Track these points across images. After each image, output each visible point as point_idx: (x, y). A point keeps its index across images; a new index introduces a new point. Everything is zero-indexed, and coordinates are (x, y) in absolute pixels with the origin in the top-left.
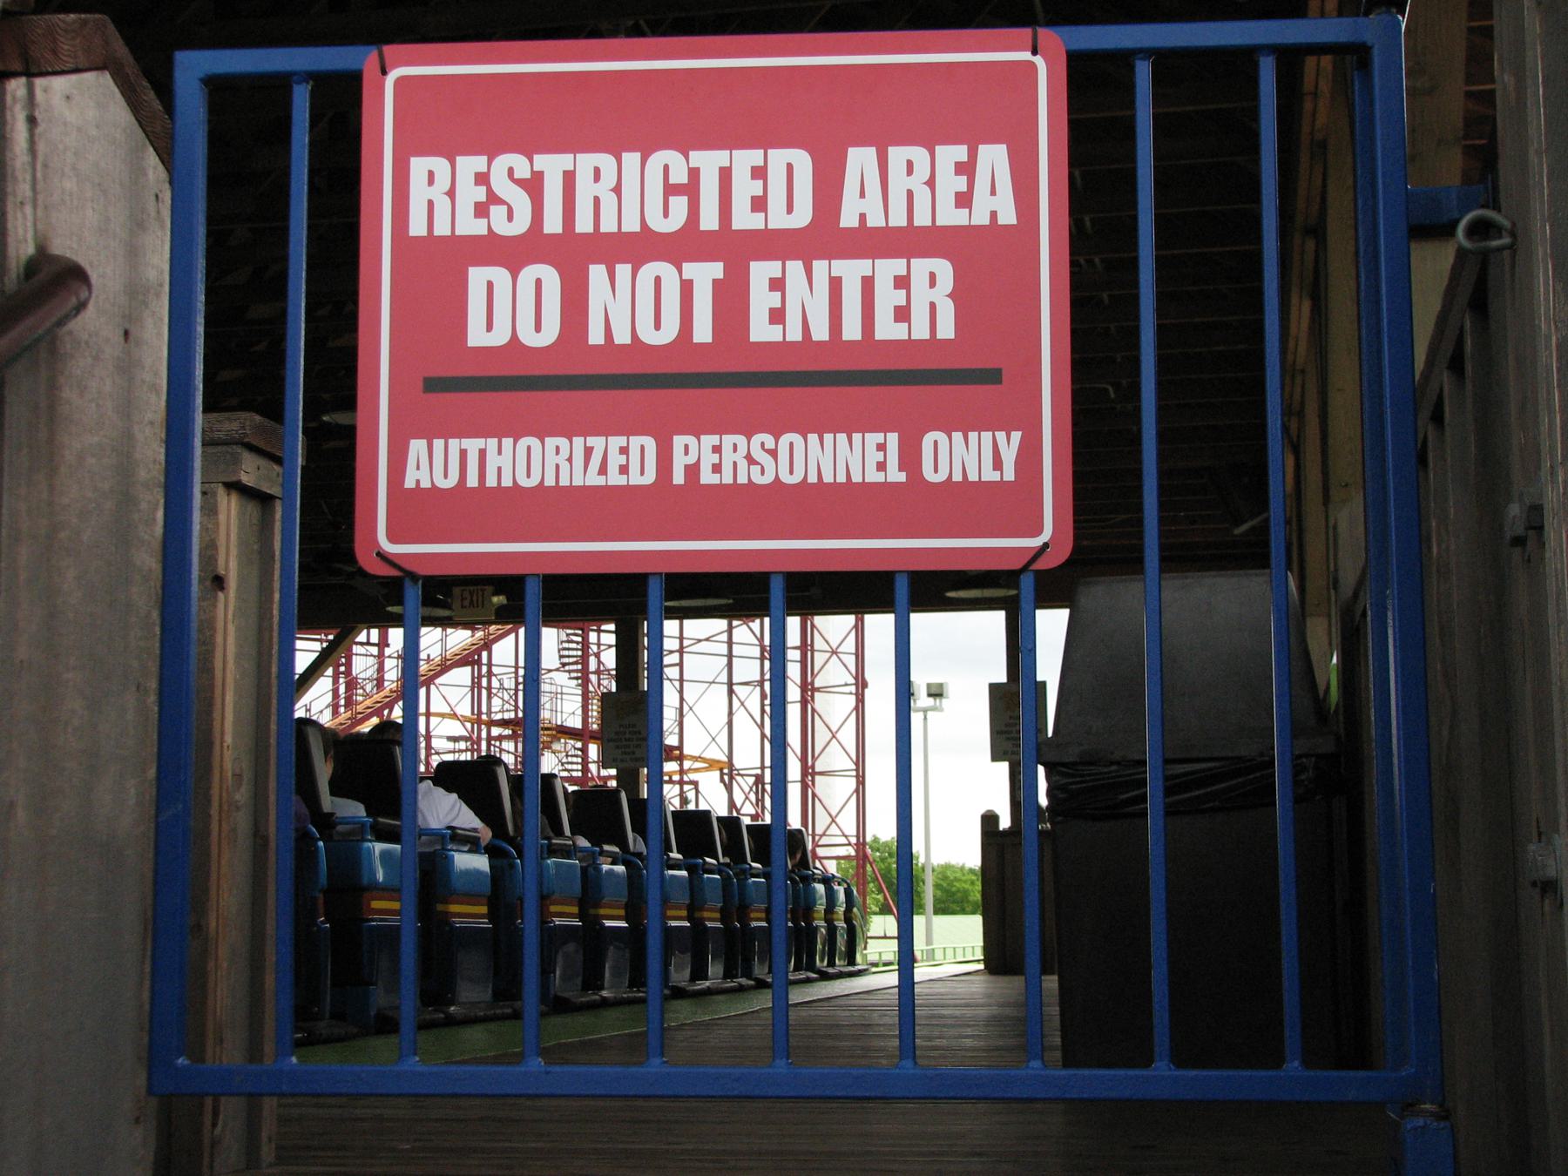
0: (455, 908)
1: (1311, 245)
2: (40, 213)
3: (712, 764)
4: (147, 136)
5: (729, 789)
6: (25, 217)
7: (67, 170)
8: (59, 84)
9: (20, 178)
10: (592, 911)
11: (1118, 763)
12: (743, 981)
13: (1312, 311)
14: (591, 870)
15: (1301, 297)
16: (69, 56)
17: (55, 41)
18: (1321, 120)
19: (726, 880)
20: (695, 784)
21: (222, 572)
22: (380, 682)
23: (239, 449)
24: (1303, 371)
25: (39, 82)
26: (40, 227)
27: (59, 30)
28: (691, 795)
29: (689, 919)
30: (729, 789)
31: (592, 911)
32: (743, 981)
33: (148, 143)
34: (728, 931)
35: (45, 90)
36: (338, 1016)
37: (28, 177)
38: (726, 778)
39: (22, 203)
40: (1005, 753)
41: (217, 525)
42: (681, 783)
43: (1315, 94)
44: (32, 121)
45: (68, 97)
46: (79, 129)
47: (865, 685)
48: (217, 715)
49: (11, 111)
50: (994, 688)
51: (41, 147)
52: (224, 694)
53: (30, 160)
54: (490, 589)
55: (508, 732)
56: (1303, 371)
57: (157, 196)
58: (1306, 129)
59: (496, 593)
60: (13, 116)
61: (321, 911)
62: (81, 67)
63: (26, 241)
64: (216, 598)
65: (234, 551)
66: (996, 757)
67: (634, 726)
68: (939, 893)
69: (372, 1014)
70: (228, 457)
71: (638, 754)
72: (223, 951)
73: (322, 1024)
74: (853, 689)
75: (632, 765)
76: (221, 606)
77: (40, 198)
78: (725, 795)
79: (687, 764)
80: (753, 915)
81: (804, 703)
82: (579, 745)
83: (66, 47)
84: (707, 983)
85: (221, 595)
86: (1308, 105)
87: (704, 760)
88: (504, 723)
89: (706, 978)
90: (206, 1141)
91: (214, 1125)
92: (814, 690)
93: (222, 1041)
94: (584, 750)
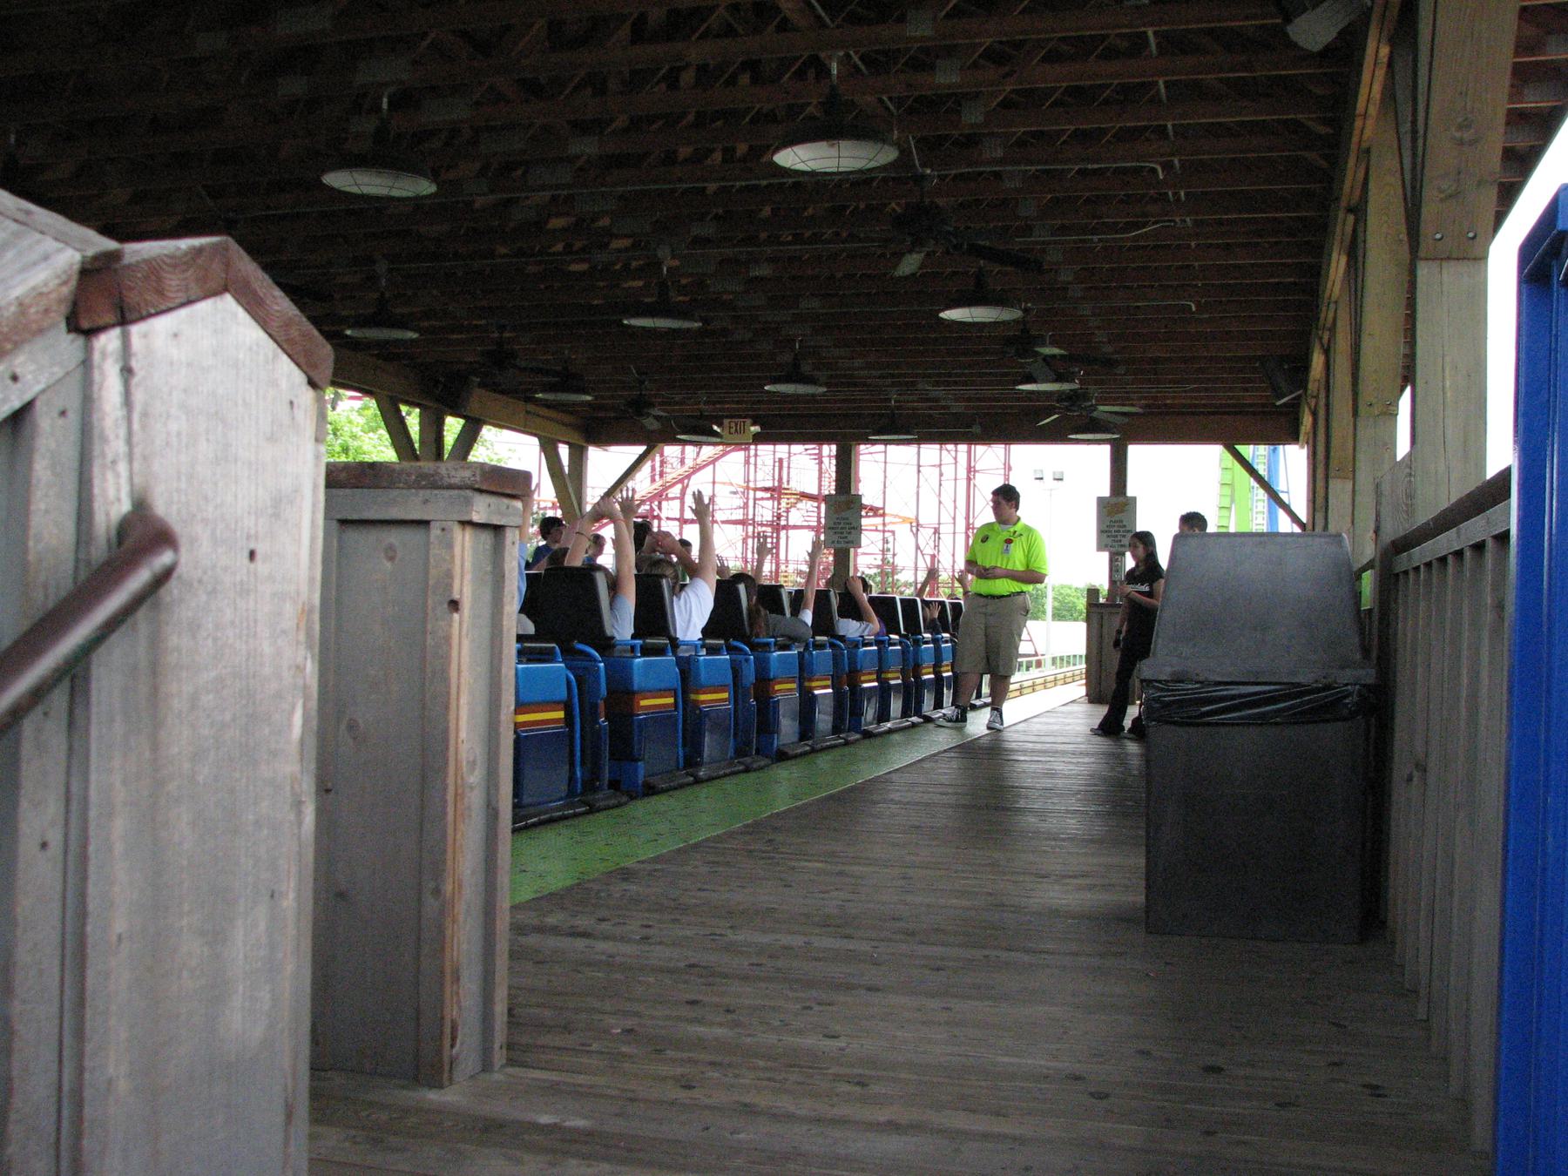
0: (703, 697)
1: (1351, 218)
2: (136, 465)
3: (905, 520)
4: (280, 346)
5: (916, 535)
6: (118, 476)
7: (174, 411)
8: (161, 325)
9: (112, 437)
10: (807, 684)
11: (1201, 682)
12: (915, 719)
13: (1348, 263)
14: (806, 655)
15: (1339, 254)
16: (178, 291)
17: (159, 279)
18: (1368, 133)
19: (904, 652)
20: (893, 532)
21: (456, 596)
22: (682, 462)
23: (469, 493)
24: (1336, 302)
25: (136, 330)
26: (137, 480)
27: (164, 267)
28: (891, 539)
29: (877, 680)
30: (916, 535)
31: (807, 684)
32: (915, 719)
33: (279, 351)
34: (906, 684)
35: (145, 336)
36: (614, 785)
37: (122, 432)
38: (914, 529)
39: (114, 462)
40: (1106, 546)
41: (453, 557)
42: (884, 531)
43: (1365, 116)
44: (127, 371)
45: (176, 335)
46: (189, 365)
47: (1010, 469)
48: (452, 716)
49: (100, 367)
50: (1100, 500)
51: (139, 397)
52: (458, 699)
53: (125, 413)
54: (749, 421)
55: (768, 495)
56: (1336, 302)
57: (291, 403)
58: (1355, 139)
59: (754, 424)
60: (102, 373)
61: (603, 714)
62: (193, 298)
63: (119, 500)
64: (451, 619)
65: (468, 577)
66: (1100, 548)
67: (847, 519)
68: (1056, 604)
69: (640, 782)
70: (462, 499)
71: (850, 538)
72: (461, 908)
73: (600, 795)
74: (1002, 472)
75: (844, 546)
76: (456, 625)
77: (137, 451)
78: (913, 540)
79: (888, 519)
80: (924, 671)
81: (969, 479)
82: (816, 504)
83: (173, 283)
84: (889, 725)
85: (456, 616)
86: (1358, 123)
87: (900, 517)
88: (766, 489)
89: (888, 721)
90: (446, 1059)
91: (452, 1046)
92: (975, 471)
93: (458, 979)
94: (819, 508)
